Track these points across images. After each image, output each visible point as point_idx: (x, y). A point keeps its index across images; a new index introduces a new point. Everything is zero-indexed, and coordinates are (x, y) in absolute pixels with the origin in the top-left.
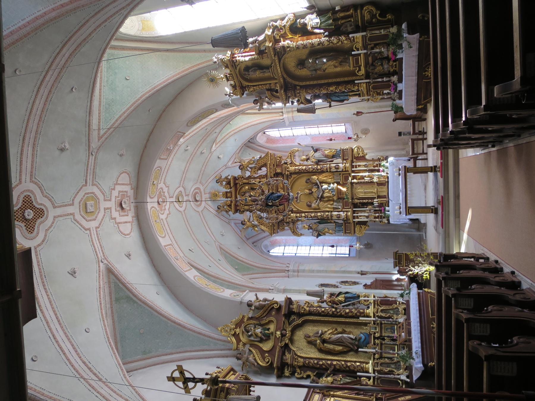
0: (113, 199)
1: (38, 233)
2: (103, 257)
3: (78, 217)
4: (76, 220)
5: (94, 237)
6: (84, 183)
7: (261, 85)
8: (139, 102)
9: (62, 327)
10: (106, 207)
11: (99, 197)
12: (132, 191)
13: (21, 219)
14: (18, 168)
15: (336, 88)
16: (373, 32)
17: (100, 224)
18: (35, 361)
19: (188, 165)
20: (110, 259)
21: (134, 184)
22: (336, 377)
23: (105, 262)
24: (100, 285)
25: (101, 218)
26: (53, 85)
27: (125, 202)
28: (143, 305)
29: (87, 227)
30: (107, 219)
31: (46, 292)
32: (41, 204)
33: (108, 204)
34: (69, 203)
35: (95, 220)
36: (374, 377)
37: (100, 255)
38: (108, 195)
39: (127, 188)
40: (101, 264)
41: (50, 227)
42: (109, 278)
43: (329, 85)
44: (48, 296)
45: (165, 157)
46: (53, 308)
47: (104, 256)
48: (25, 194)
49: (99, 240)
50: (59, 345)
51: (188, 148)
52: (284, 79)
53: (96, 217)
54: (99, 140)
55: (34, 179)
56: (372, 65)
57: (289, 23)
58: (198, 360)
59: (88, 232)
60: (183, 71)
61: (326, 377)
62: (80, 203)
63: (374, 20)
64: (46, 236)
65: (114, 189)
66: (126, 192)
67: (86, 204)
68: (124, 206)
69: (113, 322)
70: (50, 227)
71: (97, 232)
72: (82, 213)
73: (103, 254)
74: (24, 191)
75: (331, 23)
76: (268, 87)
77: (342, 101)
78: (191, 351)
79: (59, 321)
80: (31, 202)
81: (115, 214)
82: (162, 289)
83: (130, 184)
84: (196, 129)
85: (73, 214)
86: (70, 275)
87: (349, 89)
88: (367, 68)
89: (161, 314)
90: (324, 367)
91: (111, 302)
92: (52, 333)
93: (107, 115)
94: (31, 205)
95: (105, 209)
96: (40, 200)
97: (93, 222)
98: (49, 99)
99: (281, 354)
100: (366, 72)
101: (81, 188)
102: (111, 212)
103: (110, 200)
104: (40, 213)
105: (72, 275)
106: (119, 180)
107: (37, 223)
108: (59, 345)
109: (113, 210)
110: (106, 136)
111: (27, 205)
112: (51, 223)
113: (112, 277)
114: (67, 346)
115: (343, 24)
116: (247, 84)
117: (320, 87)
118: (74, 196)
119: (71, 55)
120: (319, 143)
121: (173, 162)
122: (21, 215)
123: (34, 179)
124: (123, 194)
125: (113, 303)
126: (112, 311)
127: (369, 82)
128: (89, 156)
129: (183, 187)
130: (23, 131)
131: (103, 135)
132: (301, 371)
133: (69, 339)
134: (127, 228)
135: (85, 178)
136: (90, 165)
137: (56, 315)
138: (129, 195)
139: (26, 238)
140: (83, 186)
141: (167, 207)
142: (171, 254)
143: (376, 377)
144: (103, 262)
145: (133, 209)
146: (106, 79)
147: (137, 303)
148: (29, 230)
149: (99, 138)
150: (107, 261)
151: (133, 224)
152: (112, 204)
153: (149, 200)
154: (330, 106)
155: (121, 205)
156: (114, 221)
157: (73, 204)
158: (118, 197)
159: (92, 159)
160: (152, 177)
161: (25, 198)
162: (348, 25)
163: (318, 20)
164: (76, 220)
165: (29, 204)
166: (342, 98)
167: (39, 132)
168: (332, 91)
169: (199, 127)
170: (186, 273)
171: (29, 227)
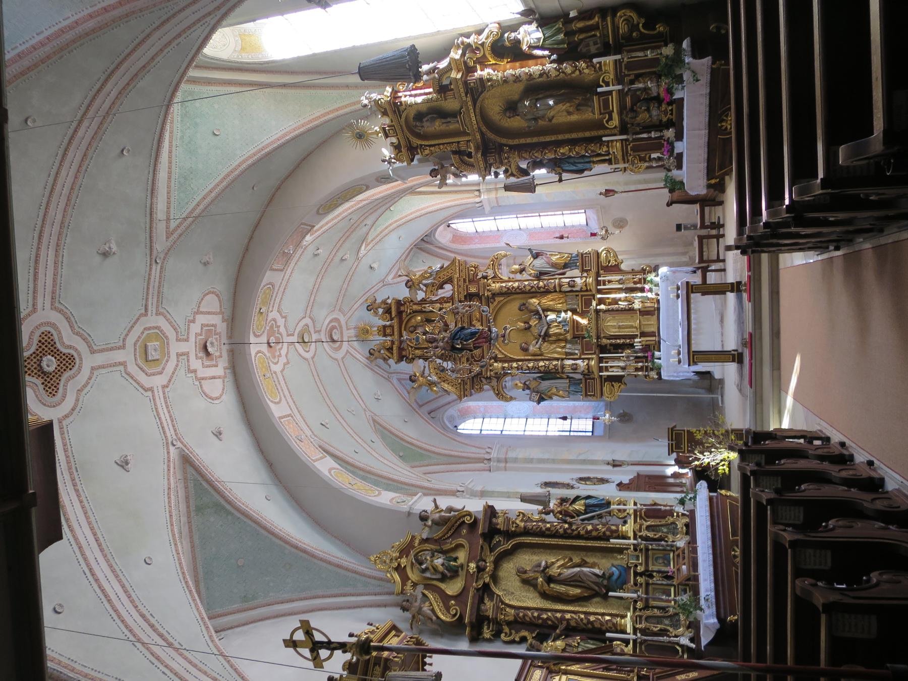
0: (192, 338)
1: (64, 396)
2: (175, 437)
3: (132, 368)
4: (128, 374)
5: (160, 402)
6: (143, 311)
7: (443, 144)
8: (237, 172)
9: (105, 556)
10: (180, 351)
11: (168, 334)
12: (225, 324)
13: (35, 371)
14: (31, 286)
15: (570, 150)
16: (634, 54)
17: (170, 381)
18: (60, 613)
19: (319, 280)
20: (186, 440)
21: (228, 313)
22: (570, 641)
23: (179, 444)
24: (169, 484)
25: (172, 370)
26: (90, 144)
27: (212, 343)
28: (242, 517)
29: (147, 386)
30: (182, 372)
31: (79, 496)
32: (70, 347)
33: (183, 347)
34: (117, 345)
35: (161, 373)
36: (635, 641)
37: (170, 433)
38: (183, 330)
39: (216, 320)
40: (172, 449)
41: (85, 386)
42: (185, 472)
43: (559, 144)
44: (81, 502)
45: (280, 267)
46: (89, 523)
48: (43, 329)
49: (167, 407)
50: (100, 587)
51: (319, 251)
52: (482, 134)
53: (163, 369)
54: (167, 238)
55: (57, 305)
56: (632, 110)
57: (490, 40)
58: (336, 612)
59: (149, 394)
60: (311, 121)
61: (554, 641)
62: (135, 344)
63: (634, 34)
64: (77, 400)
65: (193, 321)
66: (215, 326)
67: (146, 347)
68: (210, 349)
69: (193, 547)
70: (85, 386)
71: (164, 393)
72: (139, 362)
73: (175, 431)
74: (41, 324)
75: (562, 40)
76: (454, 147)
77: (581, 171)
78: (324, 597)
79: (100, 545)
80: (52, 343)
81: (196, 364)
82: (274, 491)
83: (221, 313)
84: (333, 219)
85: (123, 364)
86: (119, 467)
87: (593, 151)
88: (624, 116)
89: (273, 534)
90: (550, 623)
91: (189, 513)
92: (88, 565)
93: (181, 195)
94: (52, 348)
95: (178, 355)
96: (68, 340)
97: (158, 377)
98: (84, 168)
99: (476, 602)
100: (622, 121)
101: (138, 319)
102: (188, 361)
103: (187, 340)
105: (122, 466)
106: (202, 305)
107: (63, 379)
108: (100, 587)
109: (192, 357)
110: (179, 231)
111: (46, 349)
112: (86, 378)
113: (190, 470)
114: (113, 588)
115: (582, 40)
116: (420, 142)
117: (544, 148)
118: (125, 333)
119: (120, 93)
120: (542, 242)
121: (293, 275)
122: (35, 366)
123: (57, 305)
124: (209, 330)
125: (193, 514)
126: (190, 528)
127: (626, 140)
128: (151, 265)
129: (310, 317)
130: (39, 223)
131: (175, 230)
132: (510, 630)
133: (117, 576)
134: (215, 388)
135: (144, 302)
136: (152, 280)
137: (95, 534)
139: (45, 405)
140: (141, 315)
141: (284, 352)
142: (290, 431)
143: (639, 640)
144: (174, 445)
145: (225, 354)
146: (179, 134)
147: (232, 514)
148: (50, 390)
149: (169, 234)
150: (182, 443)
151: (226, 380)
152: (190, 347)
153: (252, 339)
154: (560, 180)
155: (205, 347)
156: (193, 375)
157: (123, 347)
158: (201, 335)
159: (156, 269)
160: (259, 301)
161: (43, 336)
162: (591, 43)
163: (540, 35)
164: (128, 374)
165: (49, 346)
166: (580, 166)
167: (66, 225)
168: (563, 154)
169: (338, 216)
170: (315, 464)
171: (49, 385)
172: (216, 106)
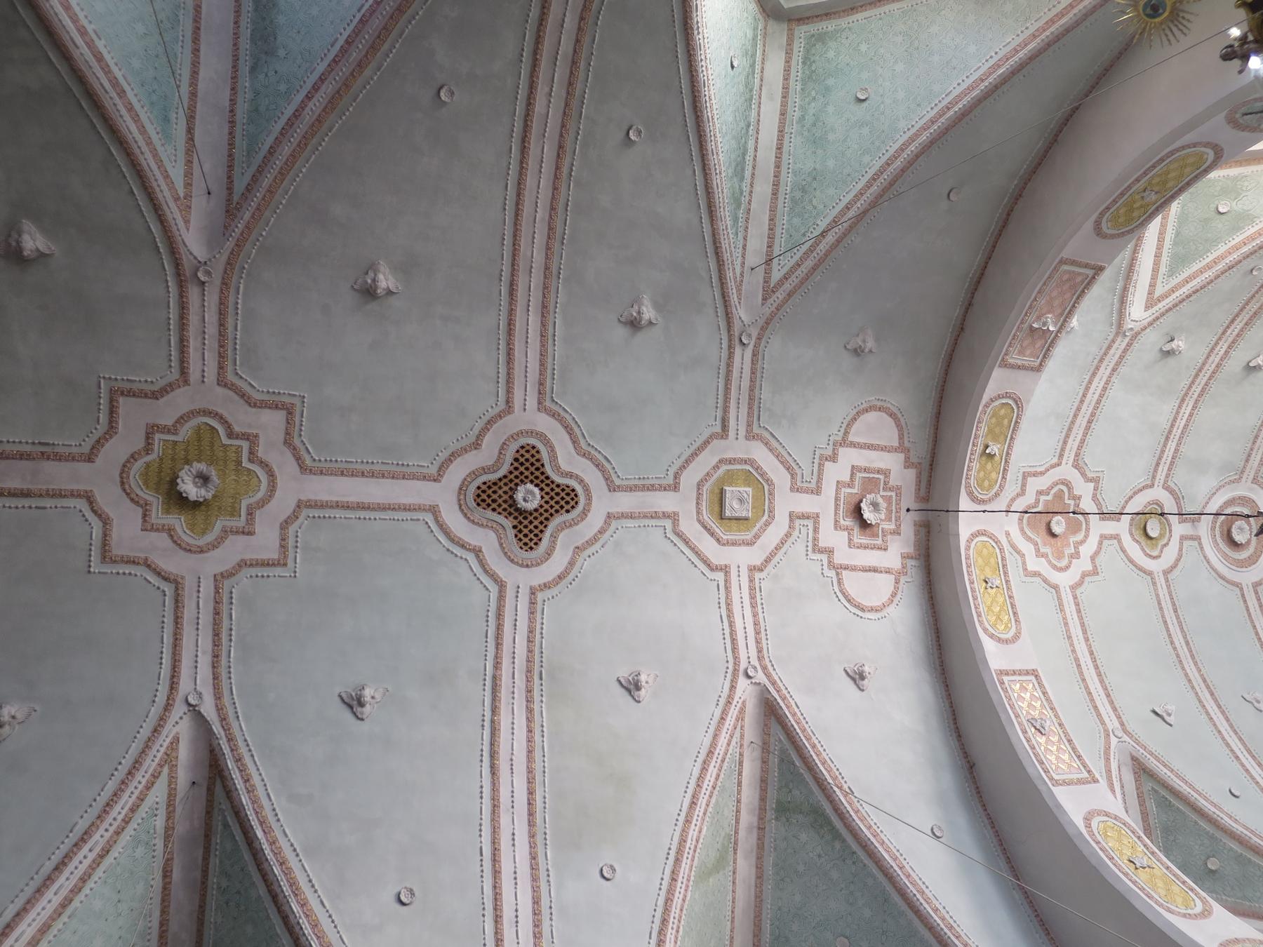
0: (829, 490)
1: (549, 554)
2: (755, 662)
3: (689, 526)
4: (679, 535)
5: (740, 595)
6: (718, 429)
8: (898, 163)
9: (532, 836)
10: (799, 509)
11: (771, 475)
12: (911, 474)
13: (505, 506)
14: (503, 370)
17: (768, 561)
18: (403, 904)
19: (1186, 410)
20: (779, 673)
21: (920, 451)
23: (760, 677)
24: (713, 744)
25: (776, 541)
26: (563, 126)
27: (875, 505)
28: (861, 854)
29: (715, 561)
30: (798, 548)
31: (530, 720)
32: (570, 475)
33: (805, 503)
34: (664, 482)
35: (750, 543)
37: (748, 653)
38: (807, 473)
39: (892, 462)
40: (742, 682)
41: (590, 543)
42: (765, 732)
44: (530, 731)
45: (1027, 360)
46: (530, 771)
47: (760, 659)
48: (523, 441)
49: (754, 606)
50: (496, 887)
51: (1174, 345)
53: (757, 537)
54: (765, 299)
55: (548, 403)
59: (720, 576)
60: (1052, 21)
62: (699, 486)
64: (572, 563)
65: (833, 458)
66: (886, 473)
67: (722, 493)
68: (868, 515)
69: (760, 876)
70: (590, 543)
71: (751, 580)
72: (705, 516)
73: (760, 651)
74: (521, 433)
79: (531, 814)
80: (538, 465)
81: (832, 537)
82: (961, 823)
83: (901, 448)
84: (1201, 271)
85: (674, 517)
86: (623, 691)
89: (917, 912)
91: (762, 809)
92: (495, 842)
93: (796, 221)
94: (537, 473)
95: (792, 517)
96: (566, 461)
97: (744, 549)
98: (565, 170)
101: (706, 443)
102: (816, 530)
103: (817, 491)
104: (562, 499)
105: (629, 691)
106: (853, 430)
107: (552, 525)
108: (496, 887)
109: (826, 524)
110: (788, 286)
111: (527, 473)
112: (595, 530)
113: (776, 729)
114: (517, 898)
118: (679, 463)
119: (582, 19)
121: (1111, 393)
122: (505, 497)
123: (548, 403)
124: (872, 481)
125: (770, 815)
126: (760, 839)
128: (730, 347)
129: (1166, 488)
130: (506, 269)
131: (781, 283)
133: (535, 879)
134: (876, 589)
135: (719, 413)
136: (735, 374)
137: (531, 792)
138: (893, 481)
139: (512, 561)
140: (713, 436)
141: (1087, 549)
142: (1020, 703)
144: (749, 677)
145: (908, 529)
146: (797, 114)
147: (844, 841)
148: (526, 540)
149: (768, 292)
150: (768, 676)
151: (903, 579)
152: (824, 504)
153: (964, 503)
155: (857, 512)
156: (824, 557)
157: (675, 487)
158: (850, 485)
159: (743, 359)
160: (980, 432)
161: (522, 452)
164: (679, 535)
165: (533, 469)
167: (555, 271)
169: (1215, 262)
170: (1056, 791)
171: (526, 531)
172: (863, 47)
